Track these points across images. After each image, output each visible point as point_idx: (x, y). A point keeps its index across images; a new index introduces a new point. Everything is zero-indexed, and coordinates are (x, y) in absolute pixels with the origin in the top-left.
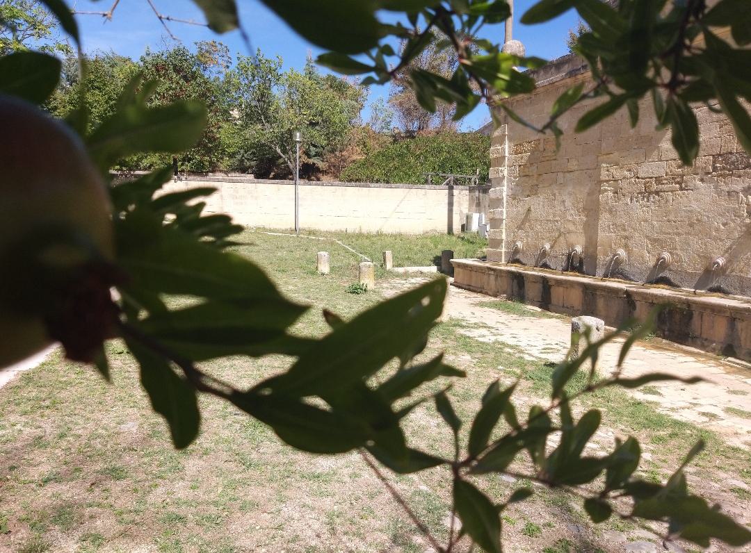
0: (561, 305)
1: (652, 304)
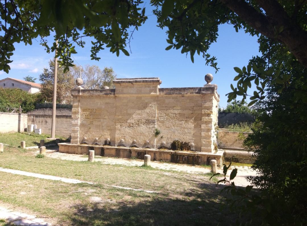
0: (108, 154)
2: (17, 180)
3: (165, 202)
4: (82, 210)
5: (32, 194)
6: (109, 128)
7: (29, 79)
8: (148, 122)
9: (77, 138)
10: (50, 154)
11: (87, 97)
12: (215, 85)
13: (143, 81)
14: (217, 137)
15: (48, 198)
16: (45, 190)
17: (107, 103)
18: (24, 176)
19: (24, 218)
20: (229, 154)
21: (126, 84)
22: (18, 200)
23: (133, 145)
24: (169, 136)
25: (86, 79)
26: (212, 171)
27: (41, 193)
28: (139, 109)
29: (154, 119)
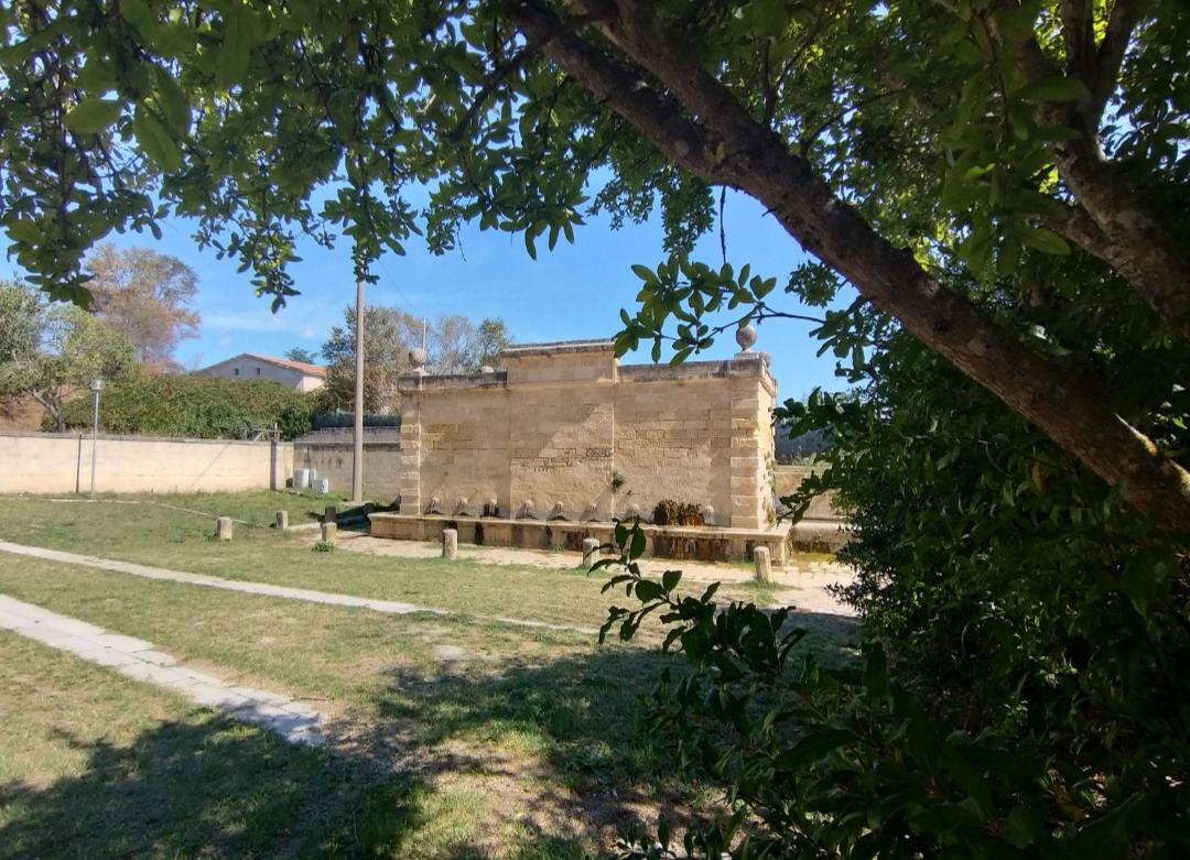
1: (564, 532)
2: (259, 608)
3: (626, 656)
4: (407, 680)
5: (290, 642)
6: (494, 473)
7: (297, 356)
8: (595, 454)
9: (413, 499)
10: (349, 542)
11: (436, 394)
12: (765, 352)
13: (577, 348)
14: (773, 490)
15: (331, 651)
16: (326, 631)
17: (485, 409)
18: (276, 596)
19: (264, 703)
20: (806, 532)
21: (535, 357)
22: (252, 657)
23: (557, 515)
24: (648, 490)
25: (436, 350)
26: (758, 577)
27: (313, 638)
28: (569, 420)
29: (609, 446)
